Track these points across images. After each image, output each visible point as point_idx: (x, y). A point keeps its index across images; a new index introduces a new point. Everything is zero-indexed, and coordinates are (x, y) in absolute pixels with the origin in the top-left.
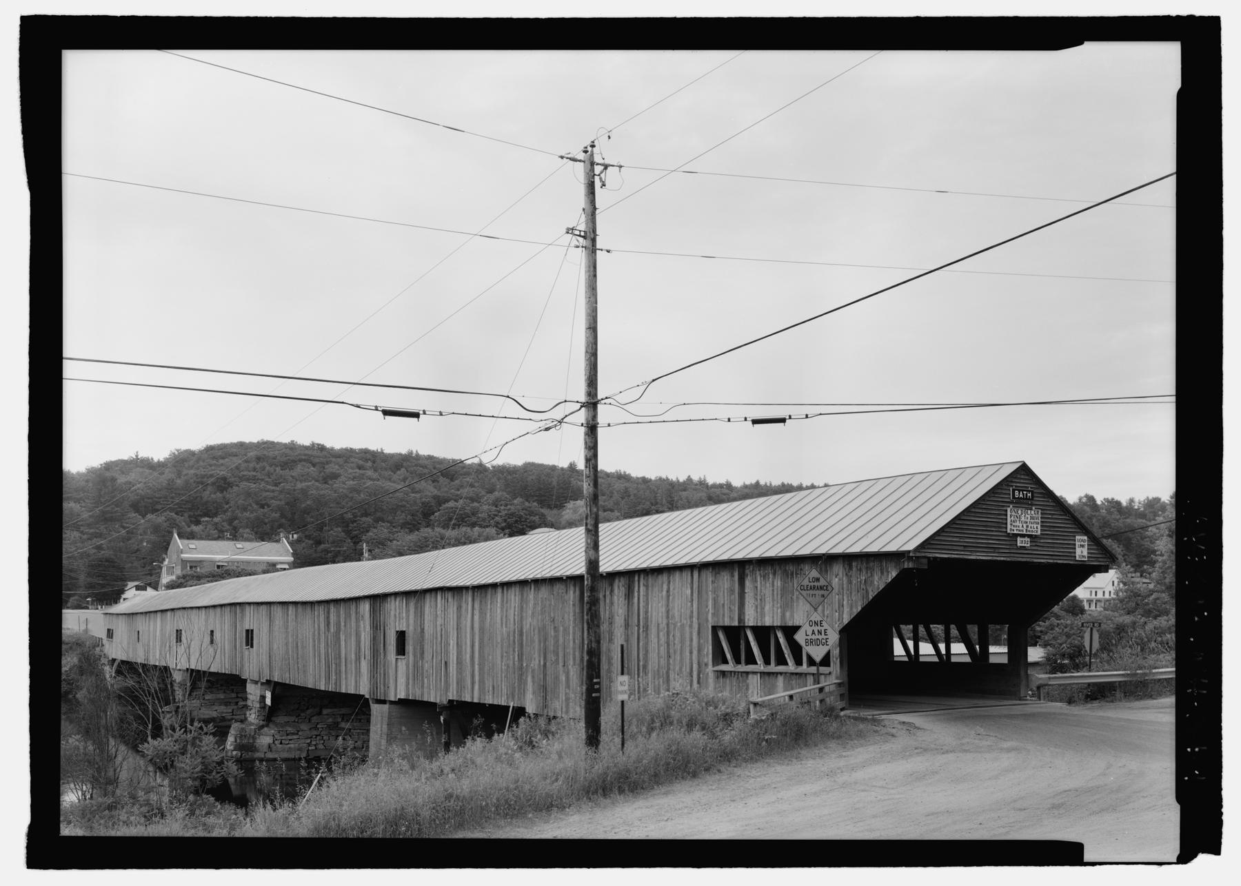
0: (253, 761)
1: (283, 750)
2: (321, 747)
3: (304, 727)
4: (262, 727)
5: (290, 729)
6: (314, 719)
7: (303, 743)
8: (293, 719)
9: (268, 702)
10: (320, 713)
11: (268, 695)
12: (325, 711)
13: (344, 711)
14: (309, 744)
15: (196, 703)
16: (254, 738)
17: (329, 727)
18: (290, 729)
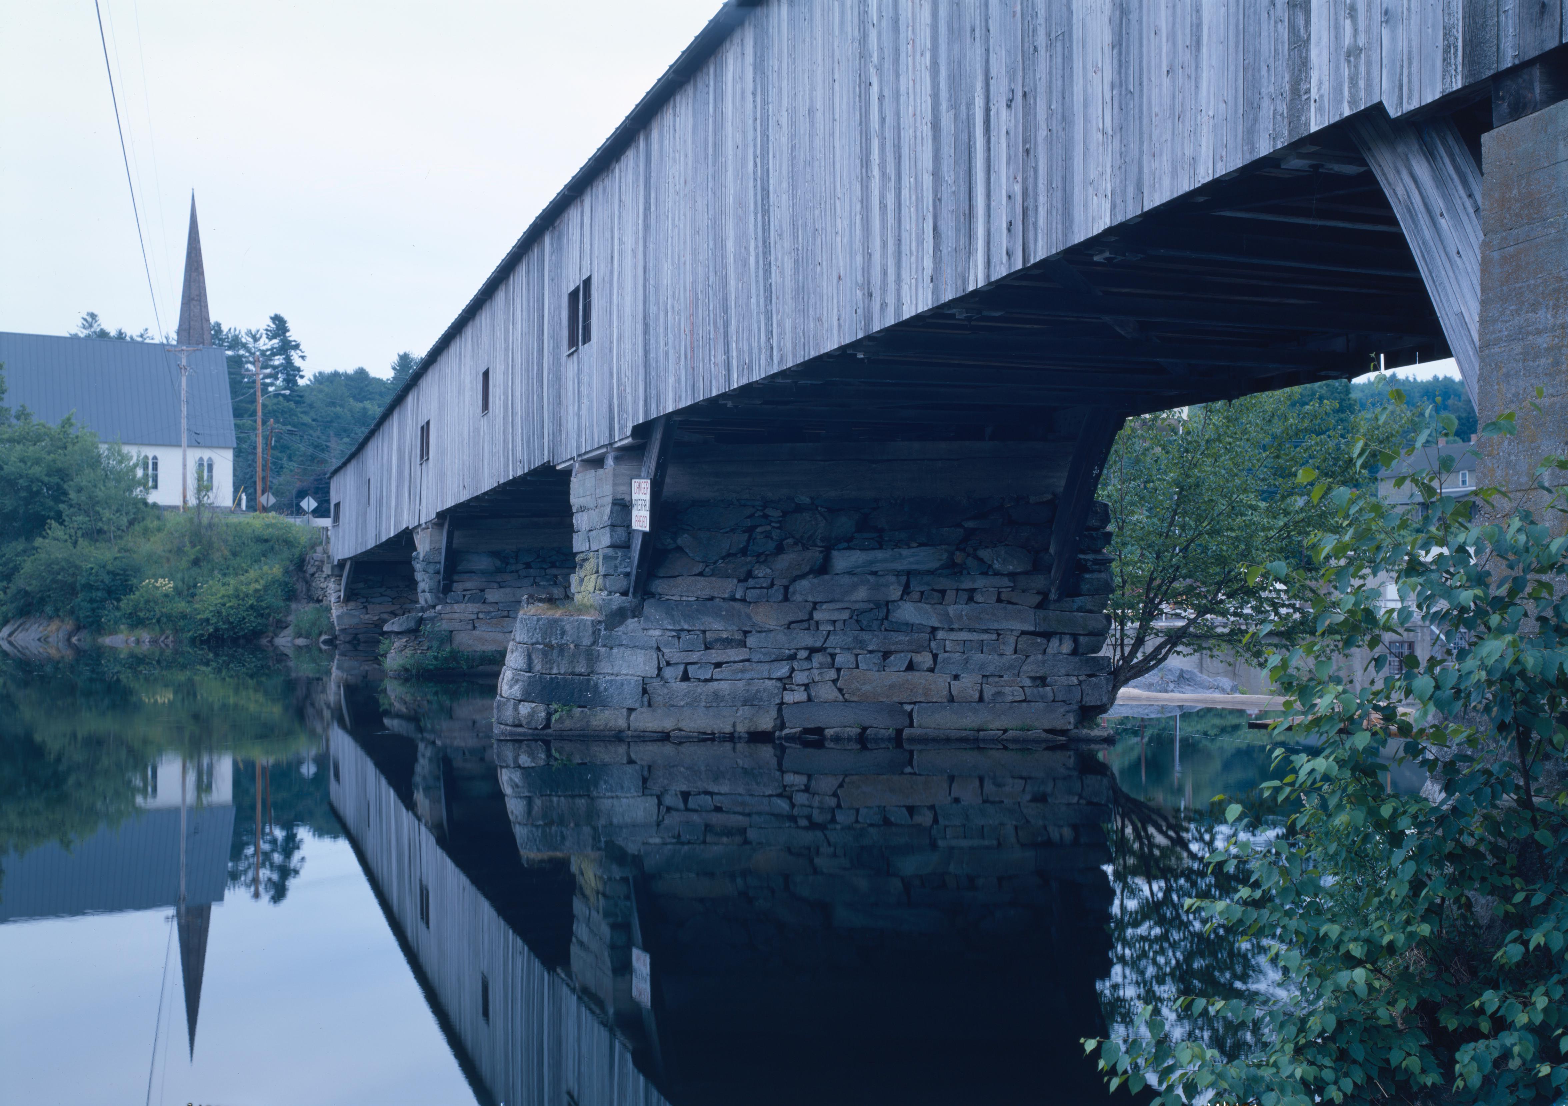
0: (588, 737)
1: (693, 703)
2: (826, 692)
3: (767, 616)
4: (617, 617)
5: (718, 627)
6: (804, 589)
7: (764, 679)
8: (727, 587)
9: (641, 519)
10: (823, 569)
11: (641, 492)
12: (842, 561)
13: (915, 557)
14: (785, 683)
15: (465, 610)
16: (592, 657)
17: (859, 620)
18: (718, 627)
